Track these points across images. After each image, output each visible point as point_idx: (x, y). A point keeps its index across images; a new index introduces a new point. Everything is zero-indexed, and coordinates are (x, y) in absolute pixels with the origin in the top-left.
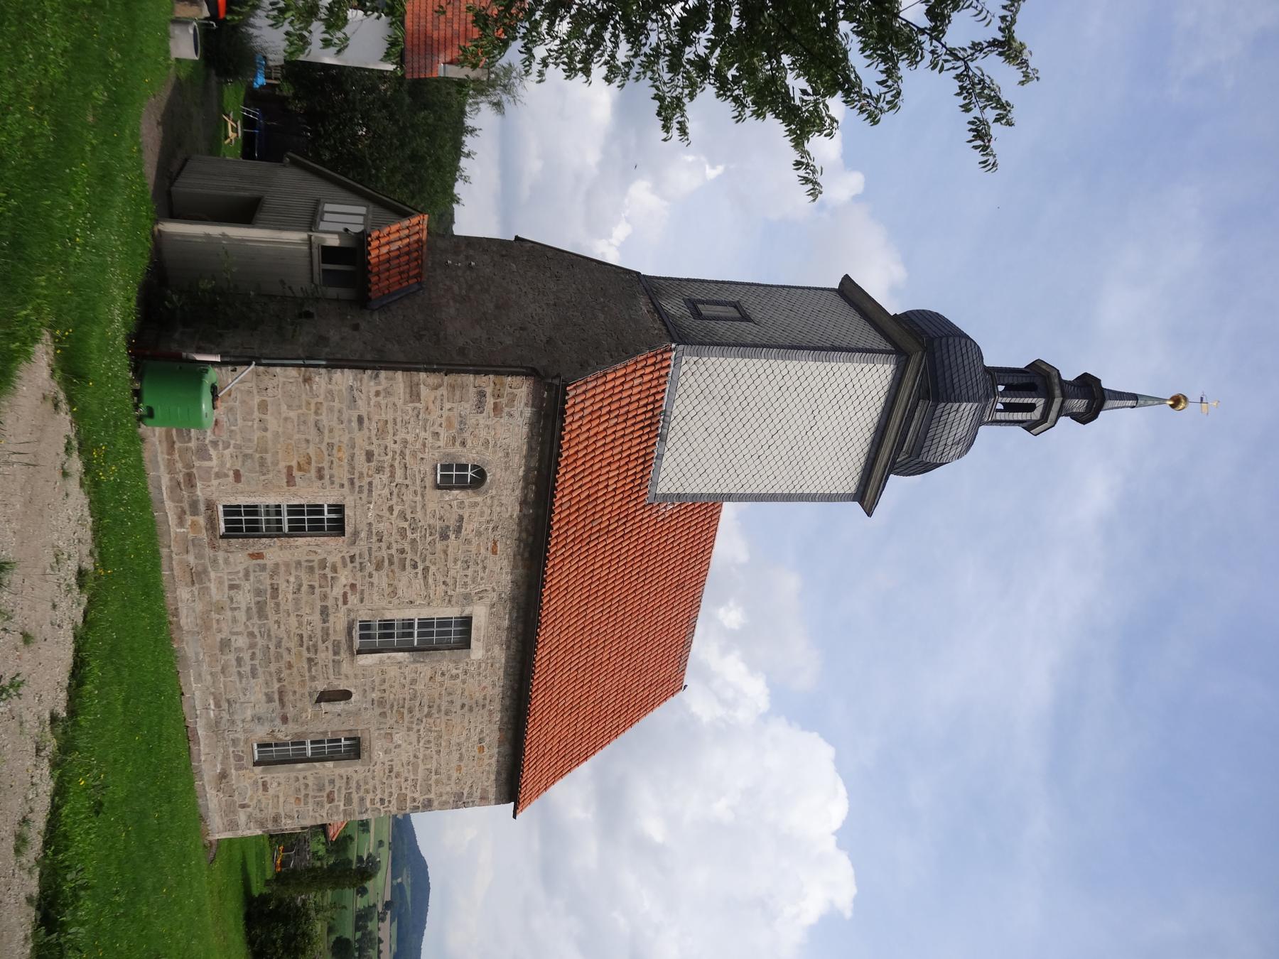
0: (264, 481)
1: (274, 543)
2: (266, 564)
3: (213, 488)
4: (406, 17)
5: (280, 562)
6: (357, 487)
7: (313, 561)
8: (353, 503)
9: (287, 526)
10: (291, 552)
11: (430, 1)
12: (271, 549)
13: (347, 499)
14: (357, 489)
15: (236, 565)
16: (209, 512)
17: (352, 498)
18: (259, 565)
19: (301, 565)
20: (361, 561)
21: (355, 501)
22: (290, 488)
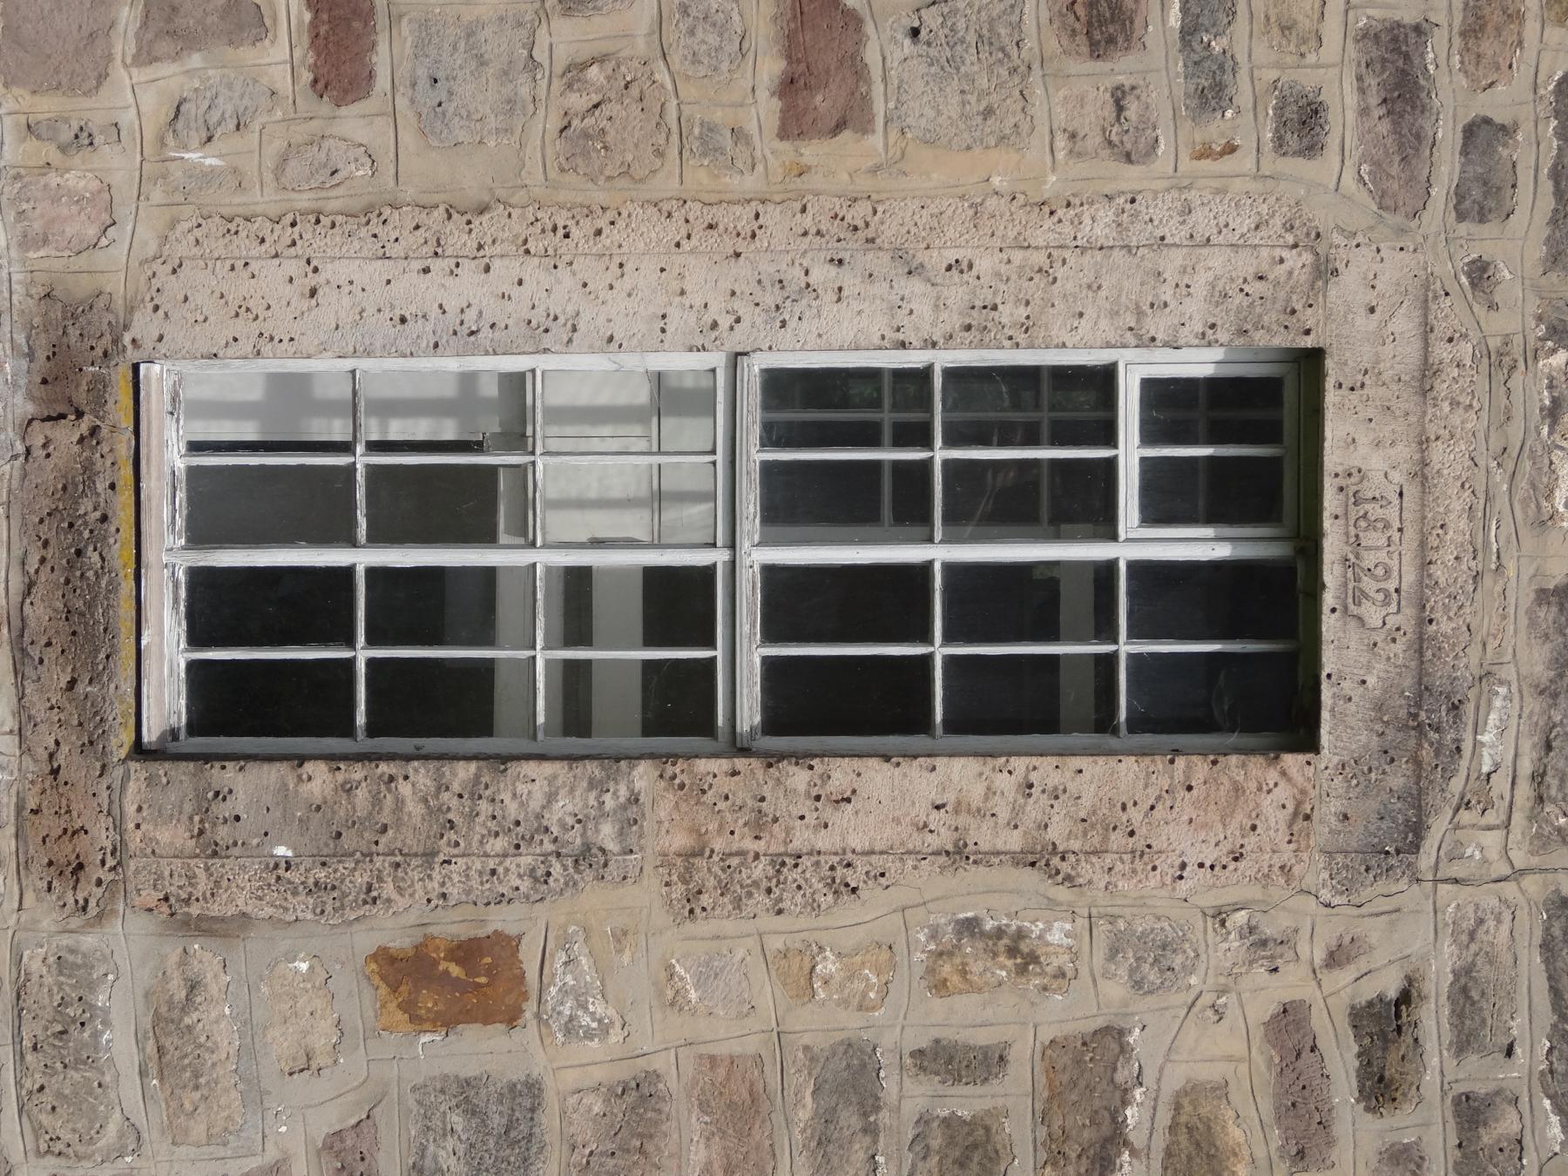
0: (575, 71)
1: (631, 816)
2: (529, 1093)
3: (118, 164)
4: (1526, 622)
5: (675, 1075)
6: (1448, 134)
7: (990, 1062)
8: (1404, 324)
9: (753, 654)
10: (781, 932)
11: (1458, 1)
12: (594, 898)
13: (1348, 288)
14: (1447, 167)
15: (255, 1095)
16: (66, 435)
17: (1395, 269)
18: (465, 1093)
19: (870, 1103)
20: (1479, 1074)
21: (1426, 296)
22: (812, 151)
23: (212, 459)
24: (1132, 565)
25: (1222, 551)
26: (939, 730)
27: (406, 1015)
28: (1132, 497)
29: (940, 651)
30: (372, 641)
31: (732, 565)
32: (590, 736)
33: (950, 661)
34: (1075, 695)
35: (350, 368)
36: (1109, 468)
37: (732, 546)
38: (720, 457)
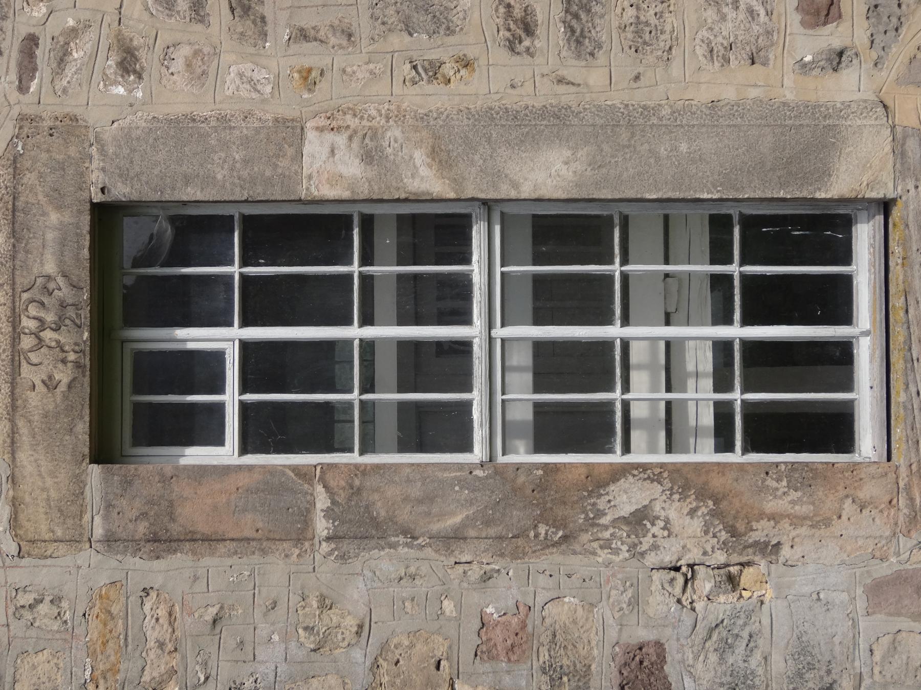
23: (603, 397)
24: (230, 324)
25: (181, 333)
26: (356, 220)
27: (266, 28)
28: (230, 369)
29: (235, 270)
30: (349, 277)
31: (491, 326)
32: (534, 216)
33: (350, 263)
34: (386, 241)
35: (505, 457)
36: (245, 388)
37: (491, 340)
38: (499, 397)
